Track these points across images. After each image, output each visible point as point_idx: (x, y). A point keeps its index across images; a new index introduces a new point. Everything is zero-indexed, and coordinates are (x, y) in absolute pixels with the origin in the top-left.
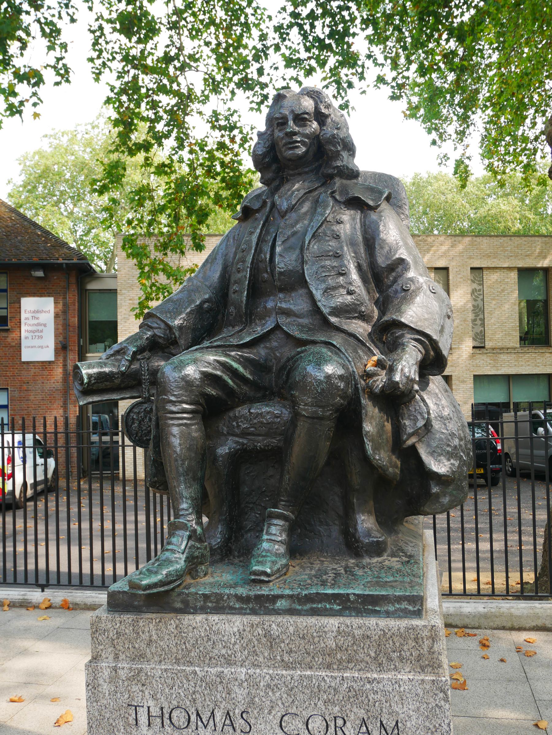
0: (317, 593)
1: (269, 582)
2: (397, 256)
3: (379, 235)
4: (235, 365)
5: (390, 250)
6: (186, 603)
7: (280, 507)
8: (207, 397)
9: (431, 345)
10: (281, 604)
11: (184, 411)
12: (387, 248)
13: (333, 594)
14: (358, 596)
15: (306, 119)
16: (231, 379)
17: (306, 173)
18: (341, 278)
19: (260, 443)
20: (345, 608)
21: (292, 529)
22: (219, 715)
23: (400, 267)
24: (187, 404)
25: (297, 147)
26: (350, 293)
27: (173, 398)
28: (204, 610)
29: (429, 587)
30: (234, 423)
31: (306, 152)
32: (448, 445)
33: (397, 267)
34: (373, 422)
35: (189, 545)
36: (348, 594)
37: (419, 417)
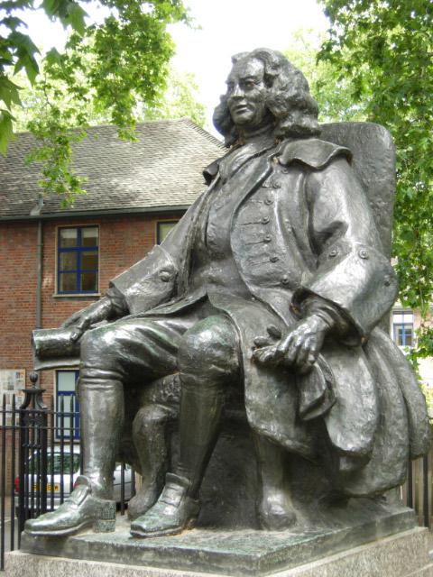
0: (175, 548)
1: (144, 537)
2: (335, 219)
3: (318, 197)
4: (161, 334)
5: (329, 215)
6: (75, 548)
7: (177, 472)
8: (121, 362)
9: (342, 314)
10: (147, 556)
11: (99, 377)
12: (325, 212)
13: (187, 550)
14: (207, 553)
15: (250, 83)
16: (154, 347)
17: (258, 135)
18: (266, 245)
20: (195, 564)
21: (191, 493)
23: (338, 231)
24: (101, 369)
25: (243, 112)
26: (274, 261)
27: (89, 364)
28: (90, 557)
29: (206, 531)
30: (162, 392)
31: (253, 117)
32: (360, 421)
33: (335, 231)
34: (259, 395)
35: (87, 499)
36: (198, 551)
37: (318, 389)
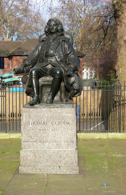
19: (46, 83)
22: (42, 122)
